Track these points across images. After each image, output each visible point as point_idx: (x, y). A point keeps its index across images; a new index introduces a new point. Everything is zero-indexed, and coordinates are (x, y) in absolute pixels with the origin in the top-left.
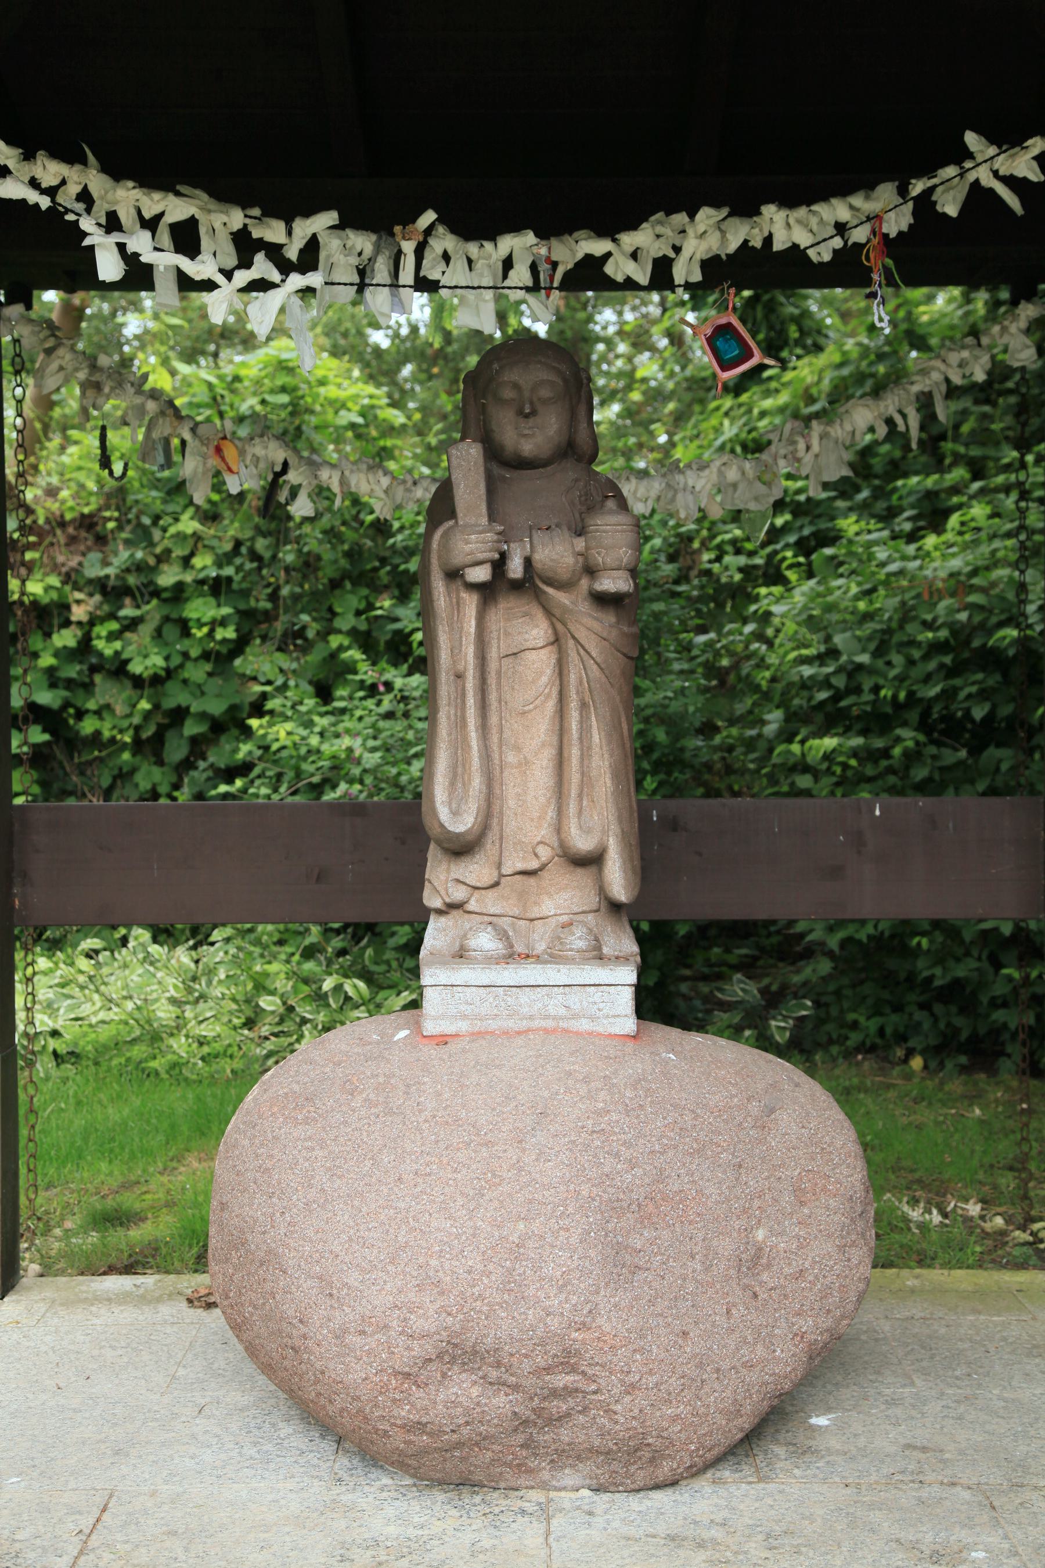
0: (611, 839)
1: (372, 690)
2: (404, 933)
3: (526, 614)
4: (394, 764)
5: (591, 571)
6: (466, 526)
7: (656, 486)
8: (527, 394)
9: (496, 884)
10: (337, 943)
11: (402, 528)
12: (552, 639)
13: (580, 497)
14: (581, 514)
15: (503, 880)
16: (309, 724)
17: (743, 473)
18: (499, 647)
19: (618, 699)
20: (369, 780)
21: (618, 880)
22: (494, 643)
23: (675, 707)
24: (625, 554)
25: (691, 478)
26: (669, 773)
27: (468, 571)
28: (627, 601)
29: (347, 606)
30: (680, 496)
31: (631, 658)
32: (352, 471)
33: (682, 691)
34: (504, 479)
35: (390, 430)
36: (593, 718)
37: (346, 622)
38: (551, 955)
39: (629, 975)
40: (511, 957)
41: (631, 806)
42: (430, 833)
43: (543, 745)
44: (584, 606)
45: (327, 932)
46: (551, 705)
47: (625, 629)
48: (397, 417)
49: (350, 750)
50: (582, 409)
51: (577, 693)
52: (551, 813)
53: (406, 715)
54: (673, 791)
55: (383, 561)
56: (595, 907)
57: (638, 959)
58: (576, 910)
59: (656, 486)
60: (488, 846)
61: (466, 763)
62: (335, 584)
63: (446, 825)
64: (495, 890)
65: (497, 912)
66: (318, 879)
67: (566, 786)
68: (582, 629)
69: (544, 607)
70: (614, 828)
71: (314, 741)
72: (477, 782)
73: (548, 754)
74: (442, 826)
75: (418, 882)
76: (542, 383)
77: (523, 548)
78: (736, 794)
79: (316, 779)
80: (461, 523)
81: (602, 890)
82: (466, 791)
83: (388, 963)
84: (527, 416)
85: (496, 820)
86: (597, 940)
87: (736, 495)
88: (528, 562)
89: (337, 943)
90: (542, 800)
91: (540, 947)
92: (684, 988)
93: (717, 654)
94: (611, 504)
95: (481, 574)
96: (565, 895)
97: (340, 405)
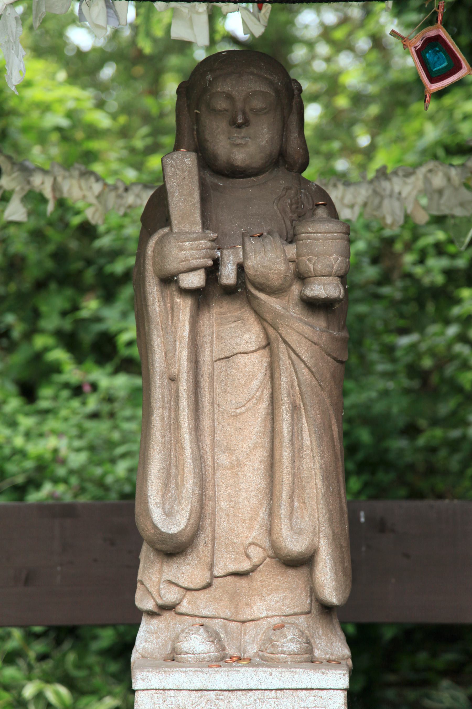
0: (322, 541)
1: (77, 391)
2: (107, 637)
3: (238, 319)
4: (100, 463)
5: (302, 277)
6: (180, 233)
7: (364, 192)
8: (239, 105)
9: (209, 585)
10: (38, 647)
11: (108, 232)
12: (264, 343)
13: (291, 205)
14: (292, 221)
15: (215, 581)
16: (12, 424)
17: (449, 179)
18: (212, 351)
19: (328, 402)
20: (74, 481)
21: (329, 581)
22: (207, 347)
23: (379, 407)
24: (335, 262)
25: (397, 185)
26: (373, 473)
27: (182, 276)
28: (337, 306)
29: (52, 306)
30: (386, 202)
31: (341, 362)
32: (64, 178)
33: (385, 393)
34: (216, 188)
35: (93, 132)
36: (304, 421)
37: (51, 322)
38: (262, 658)
39: (340, 679)
40: (223, 659)
41: (341, 508)
42: (143, 534)
43: (255, 447)
44: (296, 312)
45: (30, 637)
46: (263, 408)
47: (335, 333)
48: (102, 120)
49: (56, 451)
50: (294, 119)
51: (289, 396)
52: (263, 514)
53: (112, 415)
54: (378, 492)
55: (89, 262)
56: (306, 609)
57: (350, 662)
58: (288, 611)
59: (364, 192)
60: (201, 547)
61: (179, 465)
62: (41, 285)
63: (160, 526)
64: (207, 591)
65: (210, 614)
66: (27, 581)
67: (277, 487)
68: (294, 334)
69: (256, 312)
70: (325, 529)
71: (19, 441)
72: (190, 484)
73: (261, 455)
74: (155, 527)
75: (130, 582)
76: (255, 93)
77: (236, 255)
78: (440, 497)
79: (20, 480)
80: (175, 230)
81: (313, 592)
82: (179, 493)
83: (90, 668)
84: (239, 126)
85: (208, 522)
86: (308, 642)
87: (443, 201)
88: (241, 268)
89: (38, 647)
90: (254, 501)
91: (252, 650)
92: (391, 694)
93: (420, 356)
94: (321, 212)
95: (195, 280)
96: (277, 597)
97: (45, 108)
